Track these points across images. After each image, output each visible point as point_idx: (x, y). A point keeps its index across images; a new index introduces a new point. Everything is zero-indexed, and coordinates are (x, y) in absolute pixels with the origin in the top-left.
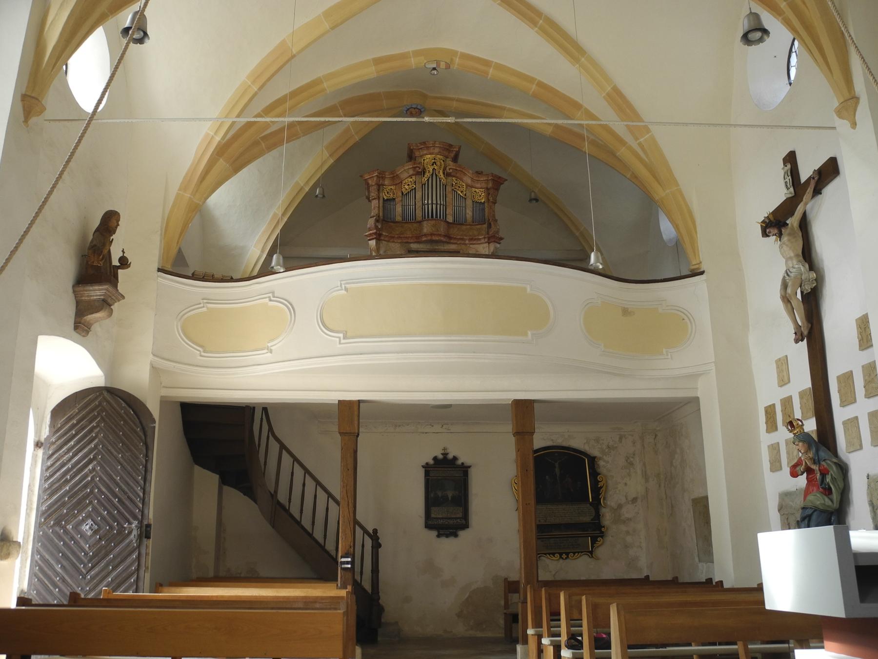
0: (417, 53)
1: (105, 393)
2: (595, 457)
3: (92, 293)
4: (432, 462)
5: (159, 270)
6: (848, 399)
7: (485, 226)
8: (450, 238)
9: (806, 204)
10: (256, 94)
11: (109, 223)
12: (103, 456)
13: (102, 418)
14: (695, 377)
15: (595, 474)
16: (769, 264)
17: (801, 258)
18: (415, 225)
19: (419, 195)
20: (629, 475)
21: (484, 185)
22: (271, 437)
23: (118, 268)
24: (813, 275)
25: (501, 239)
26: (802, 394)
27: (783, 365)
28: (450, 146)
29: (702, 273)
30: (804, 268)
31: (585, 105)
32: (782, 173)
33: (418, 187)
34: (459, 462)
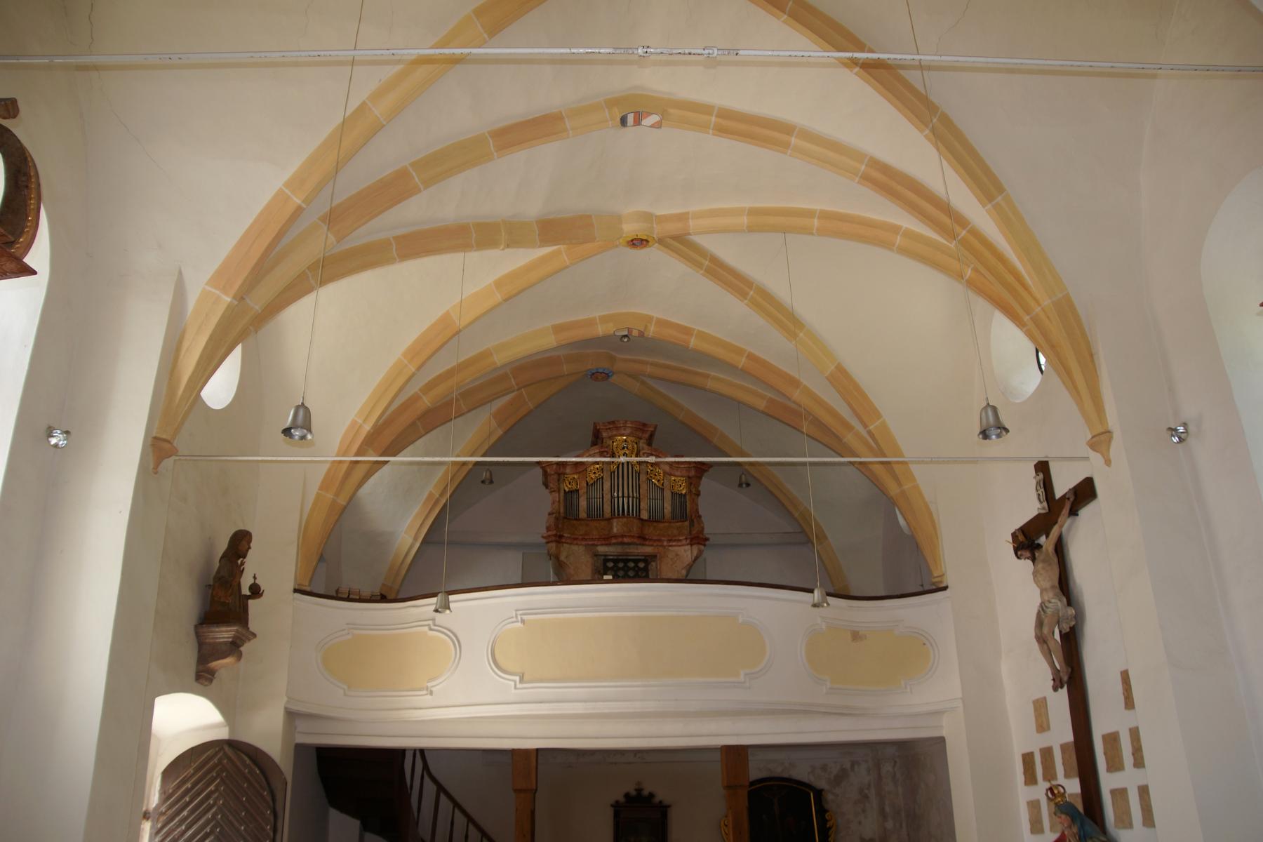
0: (605, 319)
1: (226, 748)
2: (822, 791)
3: (218, 635)
4: (622, 799)
5: (296, 591)
6: (1115, 765)
7: (687, 523)
8: (645, 539)
9: (1061, 527)
10: (413, 375)
11: (240, 543)
12: (222, 828)
13: (222, 779)
14: (939, 713)
15: (822, 811)
16: (1019, 589)
17: (1058, 590)
18: (603, 523)
19: (607, 486)
20: (864, 811)
21: (685, 473)
22: (426, 778)
23: (249, 597)
24: (1071, 611)
25: (707, 539)
26: (1064, 748)
27: (1040, 706)
28: (645, 425)
29: (945, 588)
30: (1058, 603)
31: (805, 382)
32: (1034, 482)
33: (606, 475)
34: (657, 800)
